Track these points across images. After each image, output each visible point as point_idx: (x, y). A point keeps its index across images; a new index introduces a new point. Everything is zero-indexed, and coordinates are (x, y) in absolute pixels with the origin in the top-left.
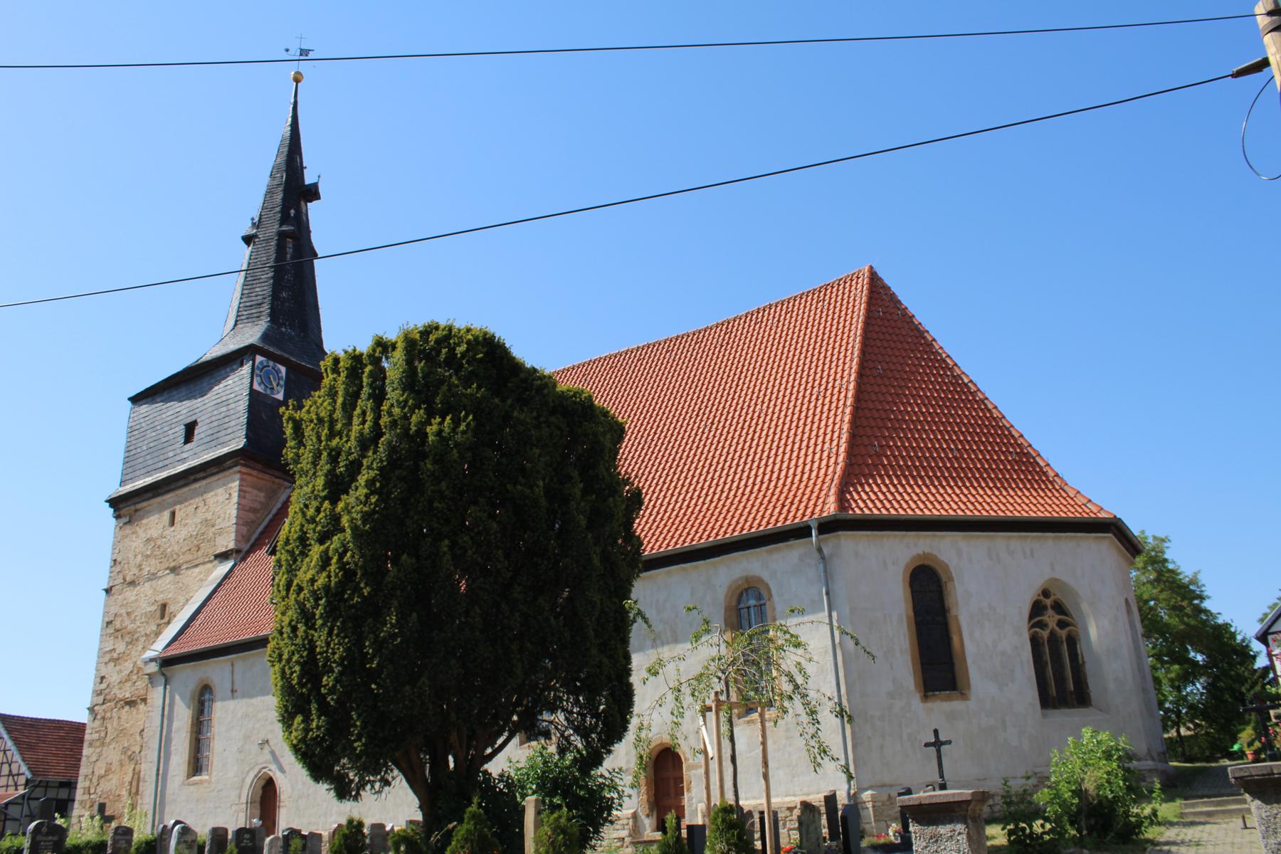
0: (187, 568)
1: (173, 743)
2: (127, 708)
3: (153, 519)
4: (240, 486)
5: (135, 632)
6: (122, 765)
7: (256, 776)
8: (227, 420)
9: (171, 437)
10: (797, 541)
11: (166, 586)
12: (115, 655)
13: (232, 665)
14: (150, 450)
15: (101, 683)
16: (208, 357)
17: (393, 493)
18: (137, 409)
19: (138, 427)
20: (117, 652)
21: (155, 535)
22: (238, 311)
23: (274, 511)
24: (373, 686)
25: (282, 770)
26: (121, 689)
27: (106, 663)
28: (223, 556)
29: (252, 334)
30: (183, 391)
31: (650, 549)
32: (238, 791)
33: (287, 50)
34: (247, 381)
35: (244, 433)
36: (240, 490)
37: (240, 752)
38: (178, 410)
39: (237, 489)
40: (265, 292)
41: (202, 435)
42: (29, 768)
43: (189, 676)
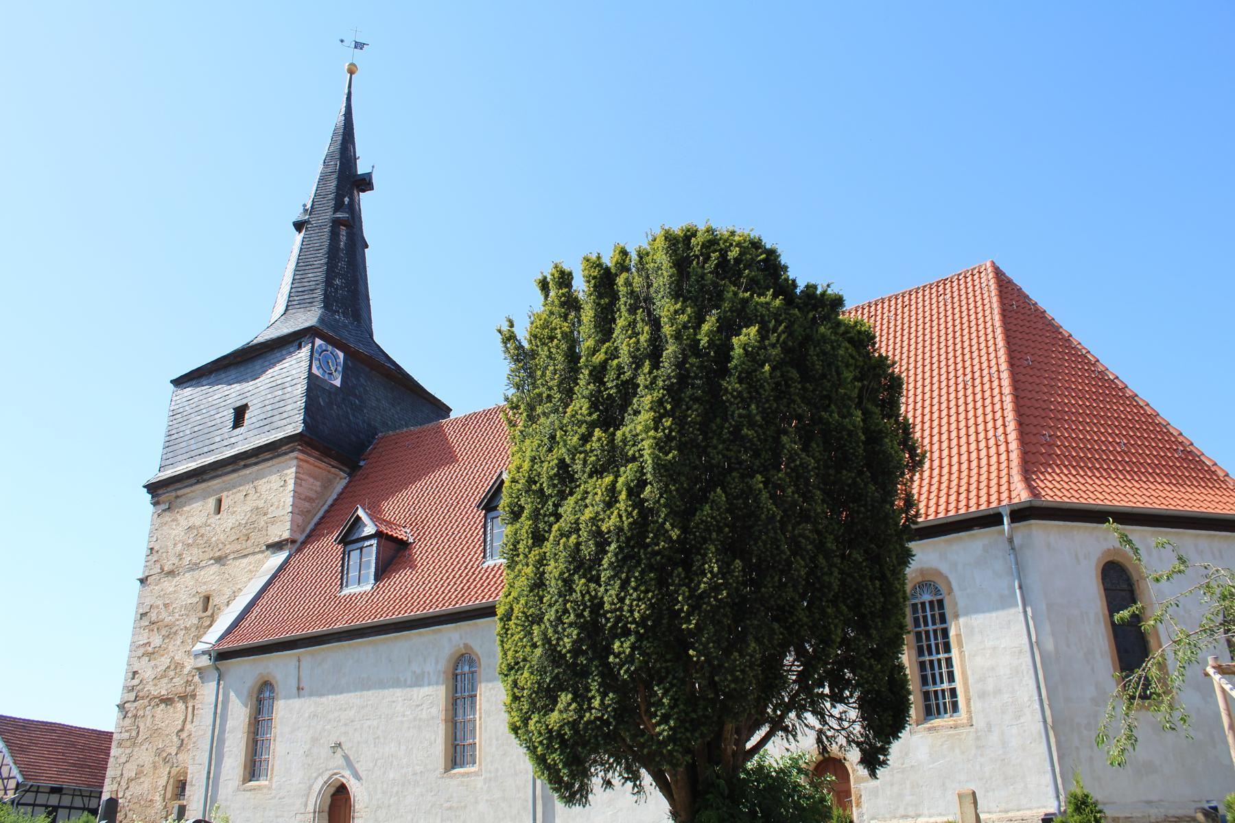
0: (234, 559)
1: (227, 744)
2: (163, 705)
3: (196, 506)
4: (296, 473)
5: (174, 624)
6: (155, 768)
7: (325, 783)
8: (282, 404)
9: (218, 421)
10: (982, 530)
11: (210, 577)
12: (150, 649)
13: (299, 661)
14: (195, 435)
15: (133, 678)
16: (260, 339)
17: (690, 416)
18: (180, 392)
19: (181, 410)
20: (152, 646)
21: (198, 523)
22: (290, 297)
23: (330, 502)
24: (691, 652)
25: (357, 777)
26: (155, 685)
27: (139, 658)
28: (277, 546)
29: (308, 318)
30: (233, 373)
31: (930, 509)
32: (304, 799)
33: (342, 41)
34: (305, 364)
35: (302, 417)
36: (296, 477)
37: (307, 756)
38: (227, 393)
39: (293, 475)
40: (318, 278)
41: (254, 420)
42: (20, 771)
43: (247, 671)
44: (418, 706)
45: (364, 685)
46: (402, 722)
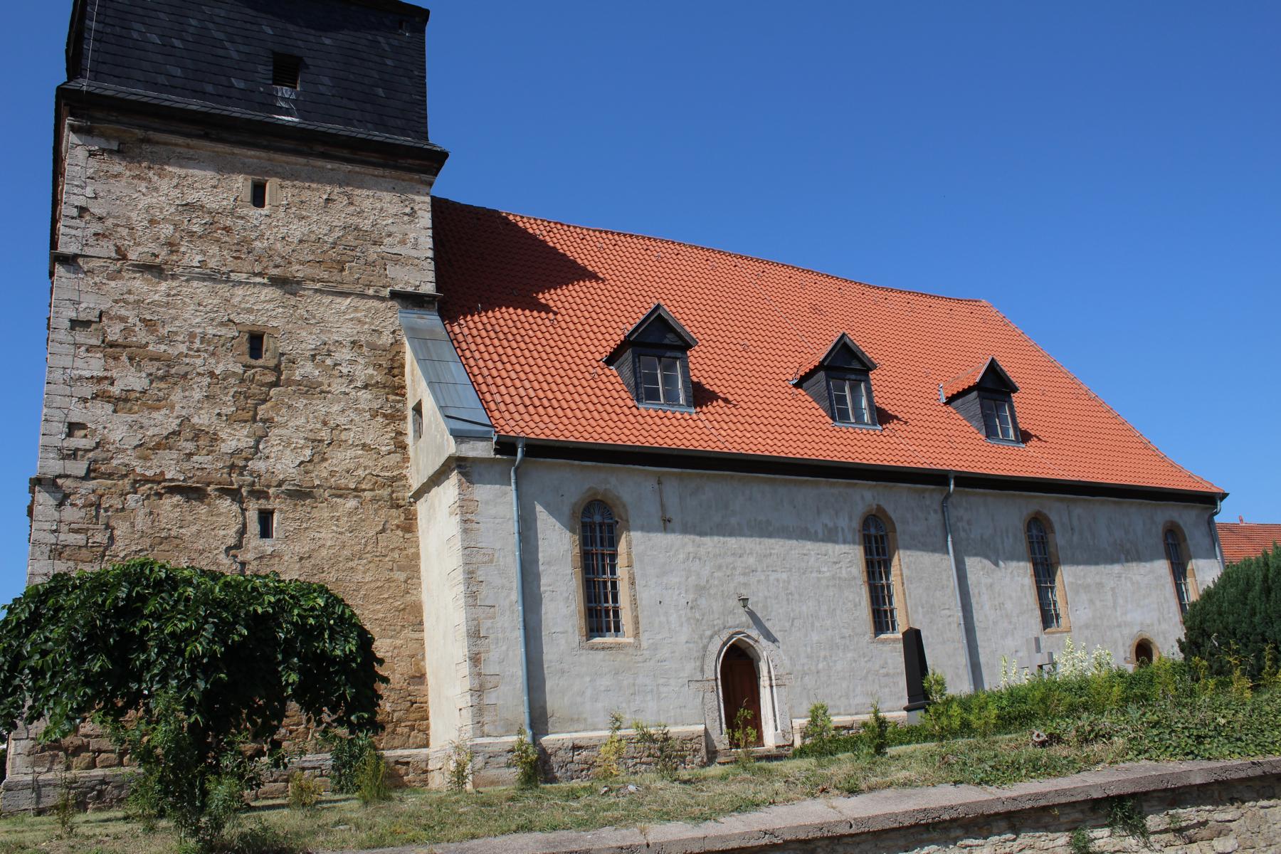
0: (316, 291)
7: (724, 644)
32: (698, 664)
37: (692, 608)
44: (835, 563)
45: (763, 530)
46: (819, 579)
